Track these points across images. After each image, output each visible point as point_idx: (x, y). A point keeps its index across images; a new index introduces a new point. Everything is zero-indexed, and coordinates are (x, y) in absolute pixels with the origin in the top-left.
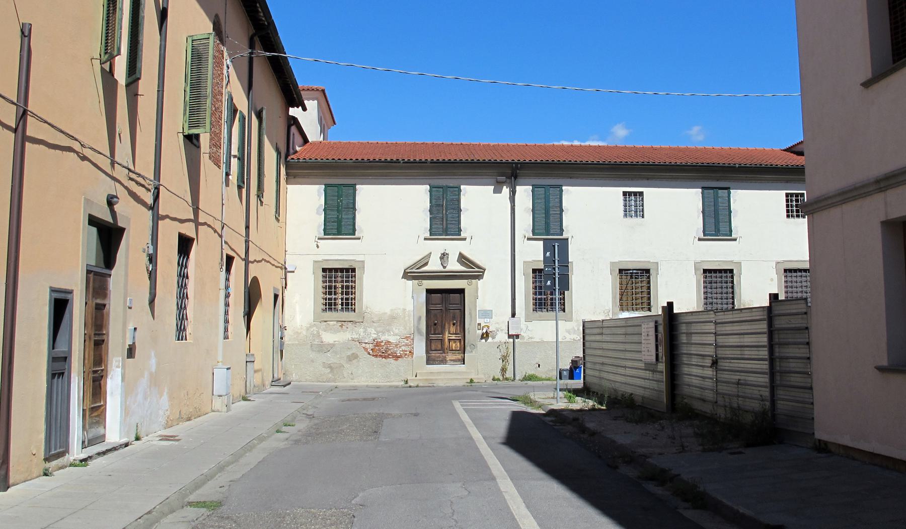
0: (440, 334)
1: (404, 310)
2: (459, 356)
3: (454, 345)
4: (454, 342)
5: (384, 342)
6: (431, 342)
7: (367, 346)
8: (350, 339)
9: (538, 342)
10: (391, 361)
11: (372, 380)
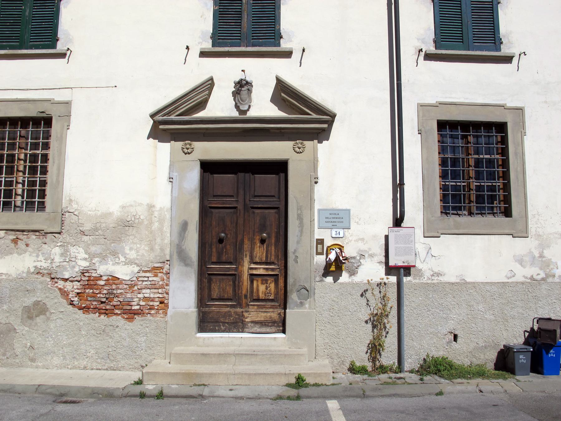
0: (230, 263)
1: (151, 207)
2: (274, 314)
3: (262, 288)
4: (264, 282)
5: (105, 278)
6: (210, 281)
7: (69, 286)
8: (32, 270)
9: (453, 284)
10: (118, 320)
11: (76, 363)
